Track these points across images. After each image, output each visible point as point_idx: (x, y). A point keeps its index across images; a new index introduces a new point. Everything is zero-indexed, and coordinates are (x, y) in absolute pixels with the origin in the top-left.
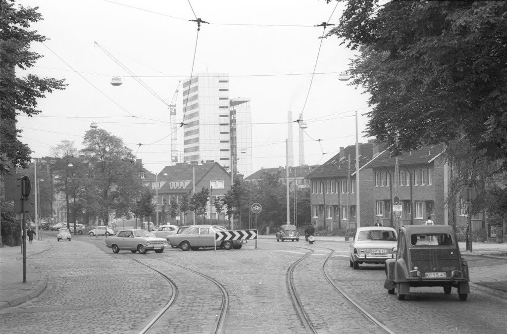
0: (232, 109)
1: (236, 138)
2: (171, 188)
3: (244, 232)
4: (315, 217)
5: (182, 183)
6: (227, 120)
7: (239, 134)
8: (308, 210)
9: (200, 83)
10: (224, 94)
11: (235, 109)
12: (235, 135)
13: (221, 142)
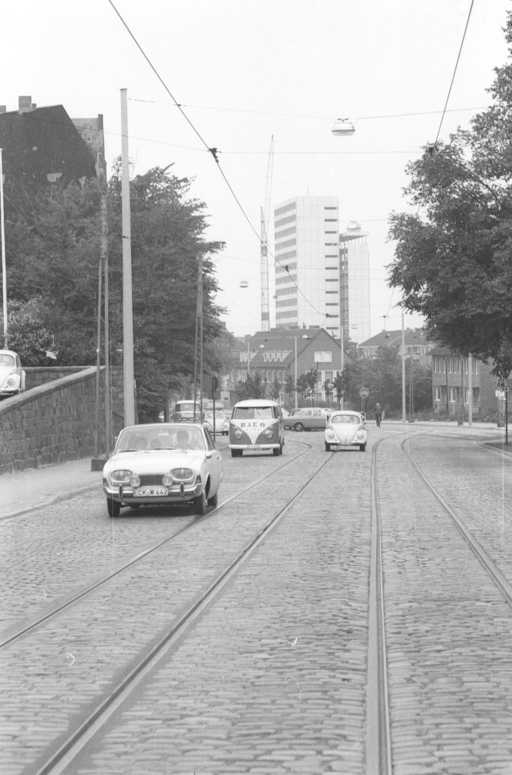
0: (342, 246)
1: (347, 287)
2: (265, 360)
4: (437, 400)
5: (279, 355)
6: (335, 262)
7: (351, 293)
8: (430, 391)
9: (299, 211)
10: (331, 226)
11: (346, 246)
12: (347, 283)
13: (327, 304)
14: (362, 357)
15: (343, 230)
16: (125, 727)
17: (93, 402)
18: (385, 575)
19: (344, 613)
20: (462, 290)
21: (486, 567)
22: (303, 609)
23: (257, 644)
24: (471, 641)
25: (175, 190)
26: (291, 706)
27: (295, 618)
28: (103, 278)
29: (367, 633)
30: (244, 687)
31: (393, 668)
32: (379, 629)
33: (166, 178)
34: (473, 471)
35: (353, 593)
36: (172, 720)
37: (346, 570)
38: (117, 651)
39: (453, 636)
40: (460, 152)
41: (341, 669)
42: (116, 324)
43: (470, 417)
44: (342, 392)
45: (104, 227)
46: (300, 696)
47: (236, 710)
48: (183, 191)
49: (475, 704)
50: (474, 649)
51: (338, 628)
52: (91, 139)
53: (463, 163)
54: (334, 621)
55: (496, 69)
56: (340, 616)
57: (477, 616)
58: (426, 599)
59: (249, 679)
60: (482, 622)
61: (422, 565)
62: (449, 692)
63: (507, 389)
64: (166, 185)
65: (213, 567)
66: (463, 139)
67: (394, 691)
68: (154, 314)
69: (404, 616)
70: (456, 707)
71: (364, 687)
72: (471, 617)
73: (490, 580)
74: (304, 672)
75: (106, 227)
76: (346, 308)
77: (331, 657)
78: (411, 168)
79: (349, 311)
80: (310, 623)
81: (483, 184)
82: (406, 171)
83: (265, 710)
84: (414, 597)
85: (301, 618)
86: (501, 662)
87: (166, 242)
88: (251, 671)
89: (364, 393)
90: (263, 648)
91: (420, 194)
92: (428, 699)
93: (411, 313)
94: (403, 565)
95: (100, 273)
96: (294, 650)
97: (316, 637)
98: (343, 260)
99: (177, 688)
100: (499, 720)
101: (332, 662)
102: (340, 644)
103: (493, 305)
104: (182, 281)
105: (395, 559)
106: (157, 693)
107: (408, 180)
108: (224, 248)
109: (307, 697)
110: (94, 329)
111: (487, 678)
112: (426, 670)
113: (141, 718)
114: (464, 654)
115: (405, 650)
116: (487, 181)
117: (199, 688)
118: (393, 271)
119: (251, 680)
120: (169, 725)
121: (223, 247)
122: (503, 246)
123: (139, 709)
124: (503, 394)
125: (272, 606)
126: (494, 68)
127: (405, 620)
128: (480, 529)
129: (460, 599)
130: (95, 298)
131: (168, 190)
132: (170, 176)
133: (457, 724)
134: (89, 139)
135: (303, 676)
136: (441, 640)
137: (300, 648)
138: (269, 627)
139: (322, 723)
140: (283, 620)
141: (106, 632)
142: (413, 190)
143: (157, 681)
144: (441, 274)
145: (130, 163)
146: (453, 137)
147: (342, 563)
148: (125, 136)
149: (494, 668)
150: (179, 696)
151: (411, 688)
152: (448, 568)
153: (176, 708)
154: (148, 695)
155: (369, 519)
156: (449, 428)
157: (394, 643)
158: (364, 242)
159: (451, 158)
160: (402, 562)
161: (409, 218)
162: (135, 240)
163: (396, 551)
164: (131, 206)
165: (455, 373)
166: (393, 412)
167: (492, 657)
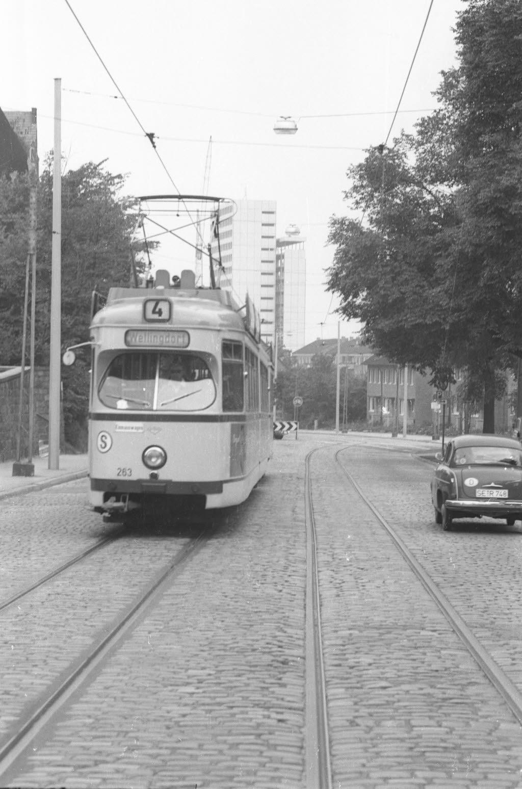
0: (279, 251)
1: (283, 293)
3: (285, 423)
6: (271, 268)
7: (287, 300)
8: (364, 402)
10: (267, 231)
11: (283, 251)
14: (296, 365)
15: (281, 235)
16: (31, 774)
17: (17, 403)
18: (322, 597)
19: (279, 641)
20: (401, 300)
21: (429, 591)
22: (234, 635)
23: (183, 675)
24: (419, 677)
25: (109, 187)
26: (221, 752)
27: (226, 645)
28: (31, 276)
29: (304, 665)
30: (168, 728)
31: (333, 707)
32: (317, 660)
33: (99, 174)
34: (410, 486)
35: (288, 617)
36: (84, 767)
37: (281, 591)
38: (27, 680)
39: (399, 671)
40: (403, 156)
41: (277, 708)
42: (43, 324)
43: (405, 429)
44: (275, 400)
45: (33, 222)
46: (230, 739)
47: (158, 755)
48: (116, 188)
49: (427, 754)
50: (423, 686)
51: (272, 658)
52: (24, 133)
53: (406, 168)
54: (267, 650)
55: (443, 73)
56: (274, 644)
57: (424, 647)
58: (367, 626)
59: (174, 718)
60: (428, 654)
61: (361, 588)
62: (398, 739)
63: (444, 402)
64: (99, 181)
65: (137, 585)
66: (407, 143)
67: (336, 736)
68: (84, 314)
69: (343, 645)
70: (406, 757)
71: (303, 730)
72: (416, 648)
73: (434, 605)
74: (235, 710)
75: (35, 221)
76: (281, 315)
77: (266, 692)
78: (353, 172)
79: (284, 318)
80: (242, 652)
81: (427, 190)
82: (348, 175)
83: (191, 756)
84: (354, 624)
85: (231, 646)
86: (453, 703)
87: (98, 241)
88: (175, 707)
89: (298, 402)
90: (190, 681)
91: (361, 199)
92: (374, 747)
93: (348, 320)
94: (341, 587)
95: (27, 269)
96: (224, 683)
97: (248, 668)
98: (279, 265)
99: (92, 727)
100: (455, 775)
101: (265, 699)
102: (274, 676)
103: (433, 315)
104: (114, 281)
105: (333, 580)
106: (69, 733)
107: (350, 183)
108: (158, 248)
109: (239, 741)
110: (20, 328)
111: (438, 722)
112: (372, 710)
113: (49, 764)
114: (411, 692)
115: (346, 685)
116: (430, 187)
117: (117, 728)
118: (331, 275)
119: (176, 719)
120: (81, 774)
121: (157, 247)
122: (446, 253)
123: (47, 752)
124: (439, 406)
125: (201, 631)
126: (440, 71)
127: (345, 650)
128: (421, 548)
129: (405, 628)
130: (22, 295)
131: (102, 187)
132: (104, 172)
133: (407, 778)
134: (22, 133)
135: (233, 715)
136: (385, 675)
137: (230, 682)
138: (197, 655)
139: (255, 774)
140: (212, 648)
141: (16, 657)
142: (354, 194)
143: (70, 717)
144: (381, 284)
145: (63, 158)
146: (396, 141)
147: (276, 583)
148: (58, 119)
149: (444, 710)
150: (95, 737)
151: (357, 732)
152: (389, 591)
153: (89, 752)
154: (59, 736)
155: (304, 534)
156: (383, 440)
157: (333, 677)
158: (302, 248)
159: (394, 162)
160: (340, 584)
161: (350, 222)
162: (66, 237)
163: (333, 571)
164: (62, 202)
165: (390, 383)
166: (326, 423)
167: (441, 696)
